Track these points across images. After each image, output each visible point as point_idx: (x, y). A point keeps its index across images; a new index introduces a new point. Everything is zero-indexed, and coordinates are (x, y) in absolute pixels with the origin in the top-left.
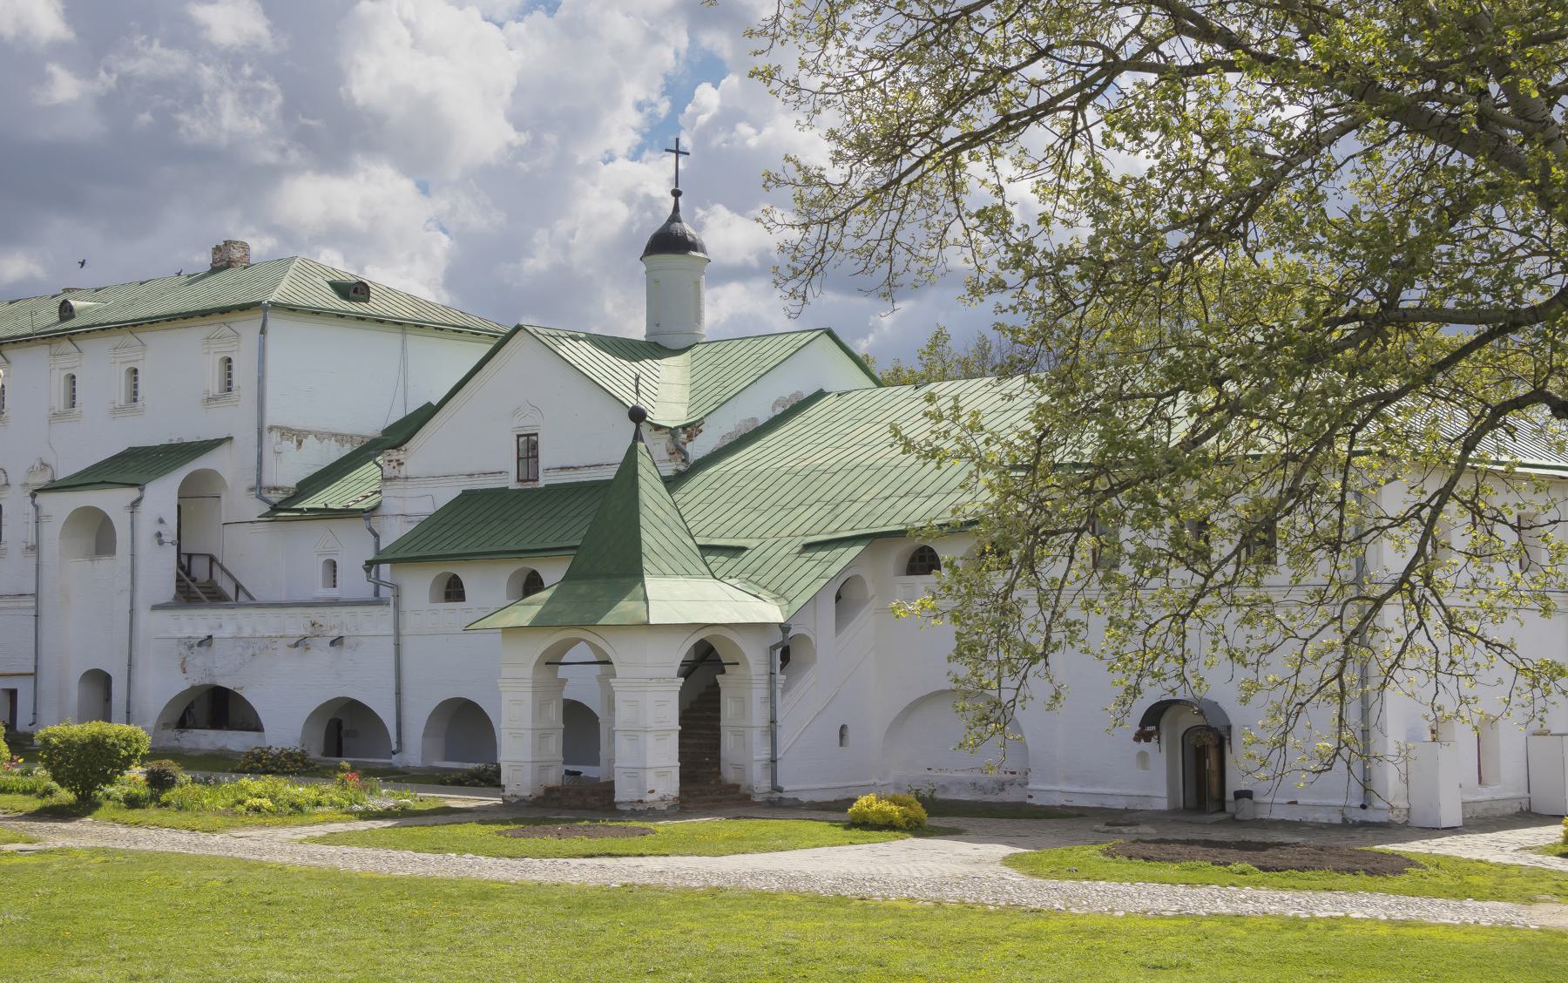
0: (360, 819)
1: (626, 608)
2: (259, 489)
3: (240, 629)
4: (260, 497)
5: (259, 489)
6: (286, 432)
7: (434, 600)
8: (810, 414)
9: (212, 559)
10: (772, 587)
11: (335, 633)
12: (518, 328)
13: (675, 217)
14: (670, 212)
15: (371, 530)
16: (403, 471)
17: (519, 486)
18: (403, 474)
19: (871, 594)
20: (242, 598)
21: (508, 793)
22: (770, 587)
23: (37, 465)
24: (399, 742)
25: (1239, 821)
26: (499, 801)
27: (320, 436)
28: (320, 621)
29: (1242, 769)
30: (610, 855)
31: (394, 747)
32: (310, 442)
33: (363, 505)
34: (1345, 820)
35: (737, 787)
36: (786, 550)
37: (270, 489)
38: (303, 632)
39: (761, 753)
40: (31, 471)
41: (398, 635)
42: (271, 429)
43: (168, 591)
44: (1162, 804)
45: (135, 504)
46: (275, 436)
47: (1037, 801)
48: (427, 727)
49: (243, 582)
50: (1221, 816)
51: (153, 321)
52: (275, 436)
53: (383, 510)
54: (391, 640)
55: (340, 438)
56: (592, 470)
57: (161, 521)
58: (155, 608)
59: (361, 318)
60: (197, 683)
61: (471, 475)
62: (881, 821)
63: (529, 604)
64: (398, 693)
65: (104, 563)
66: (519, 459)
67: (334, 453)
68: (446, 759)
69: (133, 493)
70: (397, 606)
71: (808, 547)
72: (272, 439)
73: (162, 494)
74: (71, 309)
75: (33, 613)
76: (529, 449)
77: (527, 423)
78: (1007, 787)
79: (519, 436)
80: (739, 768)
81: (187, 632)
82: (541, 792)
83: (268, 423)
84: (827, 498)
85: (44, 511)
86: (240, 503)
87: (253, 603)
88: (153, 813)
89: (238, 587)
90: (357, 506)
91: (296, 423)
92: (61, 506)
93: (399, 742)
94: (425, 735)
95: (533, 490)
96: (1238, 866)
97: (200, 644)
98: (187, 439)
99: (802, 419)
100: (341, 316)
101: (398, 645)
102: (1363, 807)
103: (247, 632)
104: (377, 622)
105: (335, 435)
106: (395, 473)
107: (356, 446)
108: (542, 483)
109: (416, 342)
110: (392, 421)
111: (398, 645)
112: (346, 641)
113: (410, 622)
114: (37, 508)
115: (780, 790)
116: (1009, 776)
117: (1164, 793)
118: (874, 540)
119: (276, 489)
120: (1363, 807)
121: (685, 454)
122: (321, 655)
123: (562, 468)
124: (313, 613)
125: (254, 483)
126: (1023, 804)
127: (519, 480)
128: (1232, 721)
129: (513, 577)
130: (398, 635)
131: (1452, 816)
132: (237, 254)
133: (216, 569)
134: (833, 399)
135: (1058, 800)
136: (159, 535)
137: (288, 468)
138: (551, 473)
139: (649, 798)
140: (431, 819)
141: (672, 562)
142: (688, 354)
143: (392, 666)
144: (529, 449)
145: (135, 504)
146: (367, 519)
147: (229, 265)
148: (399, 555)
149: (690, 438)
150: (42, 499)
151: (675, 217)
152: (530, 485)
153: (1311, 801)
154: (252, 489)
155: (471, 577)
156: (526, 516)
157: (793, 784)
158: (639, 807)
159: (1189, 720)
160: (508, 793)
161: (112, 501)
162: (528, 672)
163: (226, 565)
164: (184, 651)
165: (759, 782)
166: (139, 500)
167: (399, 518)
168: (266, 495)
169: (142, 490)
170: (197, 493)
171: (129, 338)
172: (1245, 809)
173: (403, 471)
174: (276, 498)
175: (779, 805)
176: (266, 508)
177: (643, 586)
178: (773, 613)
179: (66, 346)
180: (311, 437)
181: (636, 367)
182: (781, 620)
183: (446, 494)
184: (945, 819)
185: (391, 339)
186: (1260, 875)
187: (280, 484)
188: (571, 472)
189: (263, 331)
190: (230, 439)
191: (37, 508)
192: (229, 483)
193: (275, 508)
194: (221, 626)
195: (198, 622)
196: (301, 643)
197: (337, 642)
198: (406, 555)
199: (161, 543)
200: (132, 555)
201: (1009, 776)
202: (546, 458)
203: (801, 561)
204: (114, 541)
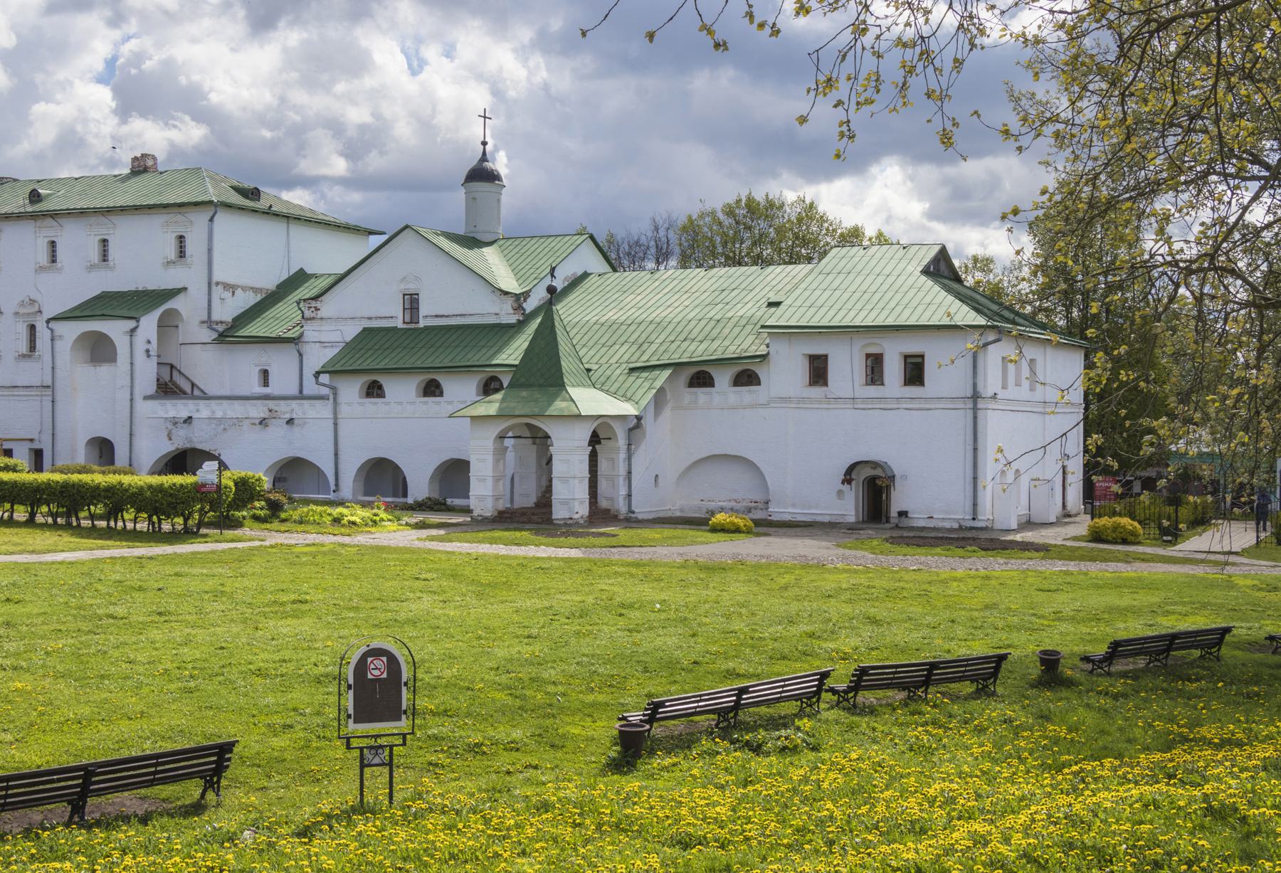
0: (416, 528)
1: (559, 406)
2: (209, 323)
3: (213, 412)
4: (210, 328)
5: (209, 323)
6: (227, 286)
7: (418, 396)
8: (587, 286)
9: (172, 367)
10: (621, 392)
11: (288, 416)
12: (407, 227)
13: (484, 158)
14: (480, 155)
15: (298, 351)
16: (320, 314)
17: (405, 326)
18: (319, 316)
19: (669, 397)
20: (196, 392)
21: (475, 514)
22: (618, 393)
23: (27, 300)
24: (337, 485)
25: (901, 528)
26: (469, 519)
27: (244, 289)
28: (275, 408)
29: (899, 500)
30: (624, 546)
31: (333, 487)
32: (239, 292)
33: (289, 335)
34: (960, 526)
35: (609, 510)
36: (618, 372)
37: (217, 323)
38: (262, 415)
39: (623, 491)
40: (22, 304)
41: (336, 418)
42: (217, 284)
43: (152, 388)
44: (852, 519)
45: (133, 330)
46: (220, 287)
47: (774, 518)
48: (356, 476)
49: (197, 382)
50: (888, 526)
51: (123, 210)
52: (220, 287)
53: (305, 338)
54: (332, 421)
55: (256, 290)
56: (459, 318)
57: (149, 342)
58: (146, 398)
59: (255, 211)
60: (180, 447)
61: (370, 318)
62: (733, 528)
63: (490, 402)
64: (336, 454)
65: (104, 370)
66: (404, 309)
67: (252, 299)
68: (366, 495)
69: (132, 324)
70: (335, 399)
71: (632, 370)
72: (217, 292)
73: (149, 324)
74: (39, 195)
75: (50, 398)
76: (412, 303)
77: (412, 288)
78: (753, 511)
79: (404, 295)
80: (611, 499)
81: (172, 414)
82: (496, 514)
83: (216, 278)
84: (632, 340)
85: (57, 333)
86: (193, 329)
87: (206, 397)
88: (276, 525)
89: (193, 385)
90: (285, 335)
91: (231, 281)
92: (71, 331)
93: (337, 485)
94: (355, 481)
95: (415, 329)
96: (969, 548)
97: (185, 422)
98: (150, 288)
99: (583, 290)
100: (241, 209)
101: (336, 424)
102: (974, 519)
103: (219, 414)
104: (322, 411)
105: (252, 288)
106: (313, 315)
107: (264, 296)
108: (422, 324)
109: (297, 232)
110: (282, 280)
111: (336, 424)
112: (296, 422)
113: (344, 410)
114: (52, 331)
115: (633, 513)
116: (753, 504)
117: (853, 513)
118: (678, 366)
119: (222, 322)
120: (974, 519)
121: (524, 310)
122: (277, 431)
123: (437, 316)
124: (271, 404)
125: (205, 318)
126: (766, 520)
127: (404, 323)
128: (896, 473)
129: (421, 382)
130: (336, 418)
131: (1014, 526)
132: (150, 163)
133: (175, 374)
134: (595, 279)
135: (787, 518)
136: (148, 351)
137: (227, 310)
138: (429, 319)
139: (576, 516)
140: (459, 528)
141: (613, 378)
142: (495, 245)
143: (331, 438)
144: (412, 303)
145: (133, 330)
146: (296, 344)
147: (145, 170)
148: (338, 367)
149: (525, 300)
150: (53, 325)
151: (484, 158)
152: (412, 326)
153: (941, 517)
154: (203, 322)
155: (389, 384)
156: (420, 345)
157: (642, 509)
158: (569, 522)
159: (868, 472)
160: (475, 514)
161: (115, 329)
162: (491, 441)
163: (182, 370)
164: (170, 426)
165: (622, 507)
166: (136, 327)
167: (317, 344)
168: (215, 326)
169: (138, 321)
170: (168, 324)
171: (102, 219)
172: (905, 522)
173: (320, 314)
174: (221, 328)
175: (630, 521)
176: (215, 335)
177: (567, 392)
178: (629, 409)
179: (49, 221)
180: (239, 289)
181: (103, 232)
182: (636, 413)
183: (351, 331)
184: (26, 561)
185: (279, 227)
186: (983, 553)
187: (223, 320)
188: (443, 319)
189: (211, 220)
190: (185, 289)
191: (52, 331)
192: (184, 317)
193: (221, 335)
194: (198, 411)
195: (178, 409)
196: (263, 422)
197: (290, 422)
198: (335, 370)
199: (149, 356)
200: (132, 364)
201: (753, 504)
202: (424, 310)
203: (632, 379)
204: (116, 354)
